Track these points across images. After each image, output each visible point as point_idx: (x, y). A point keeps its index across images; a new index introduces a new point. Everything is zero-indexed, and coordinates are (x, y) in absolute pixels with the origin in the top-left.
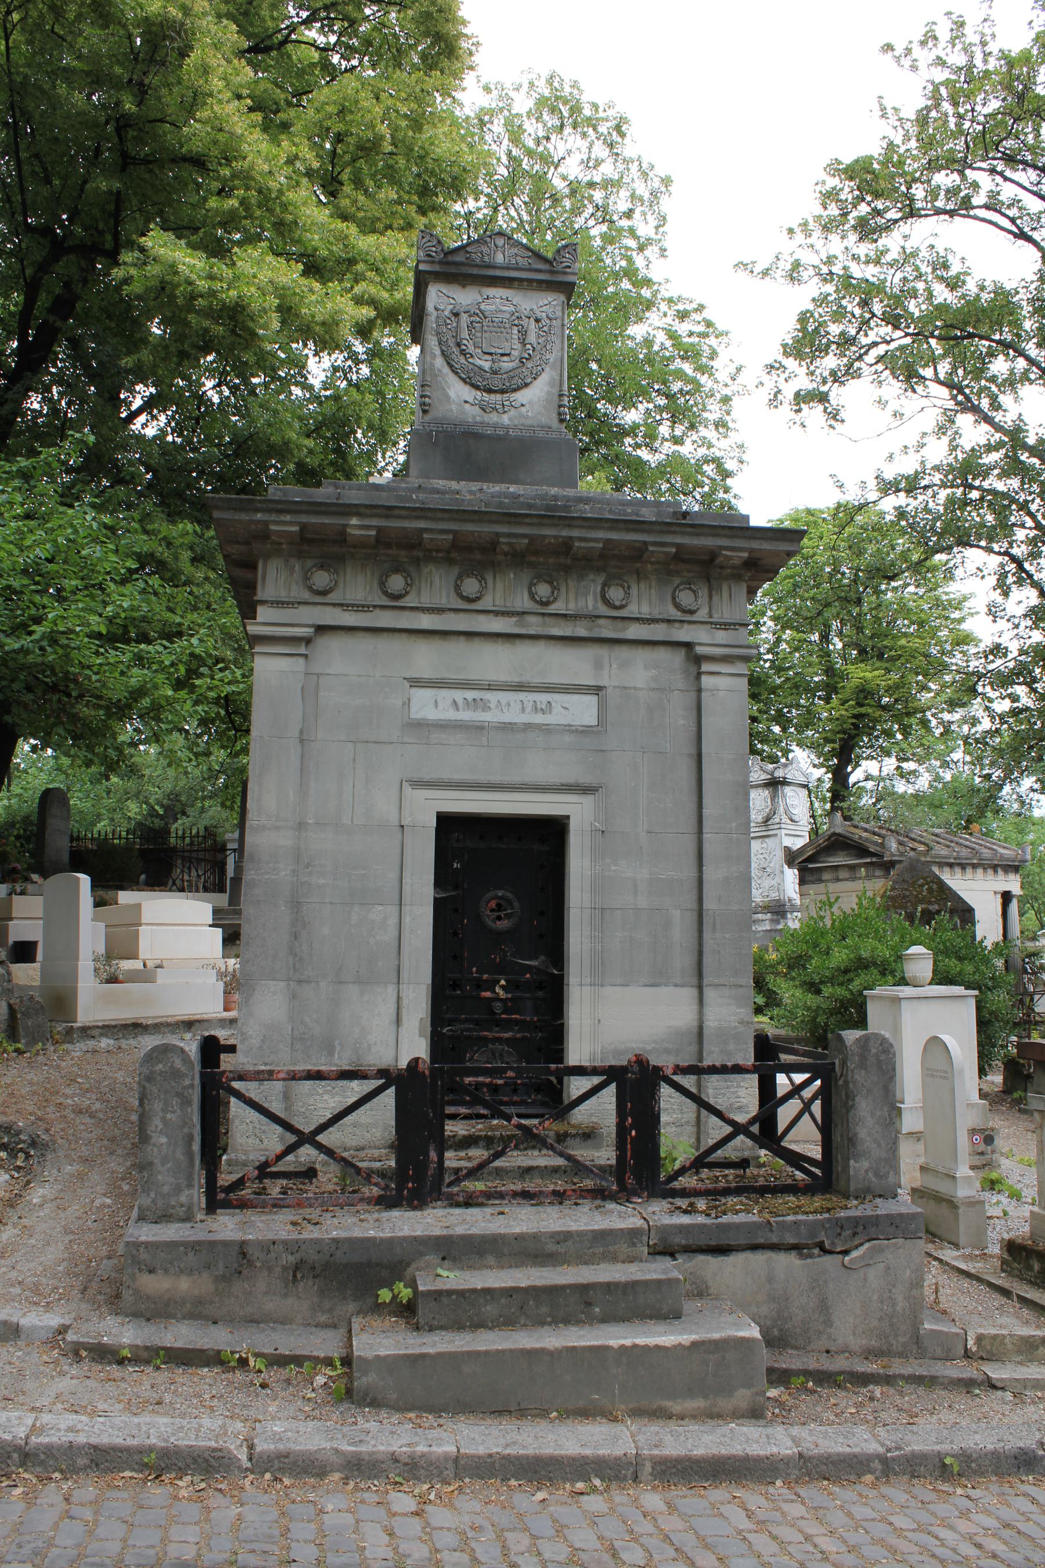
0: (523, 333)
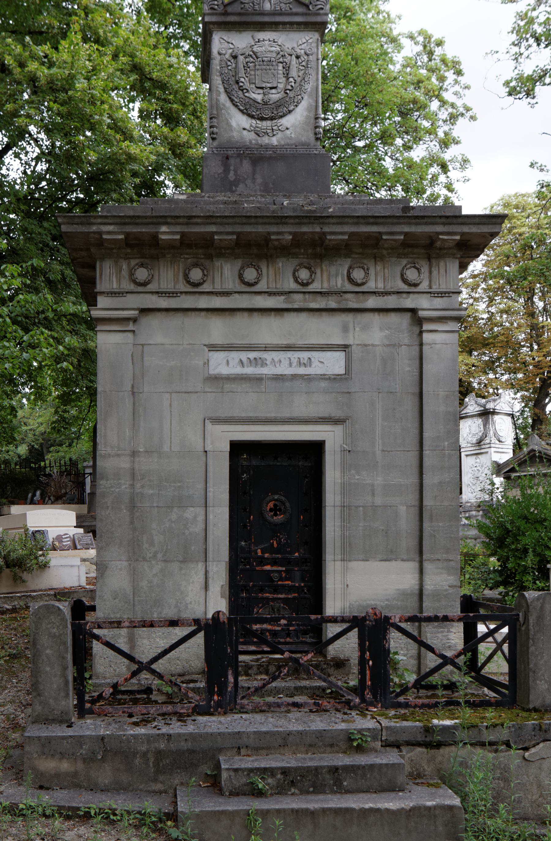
0: (287, 69)
